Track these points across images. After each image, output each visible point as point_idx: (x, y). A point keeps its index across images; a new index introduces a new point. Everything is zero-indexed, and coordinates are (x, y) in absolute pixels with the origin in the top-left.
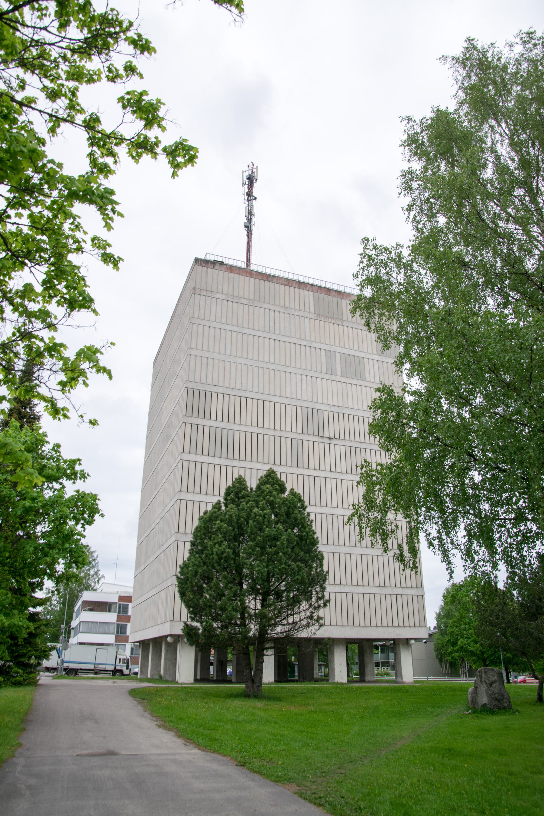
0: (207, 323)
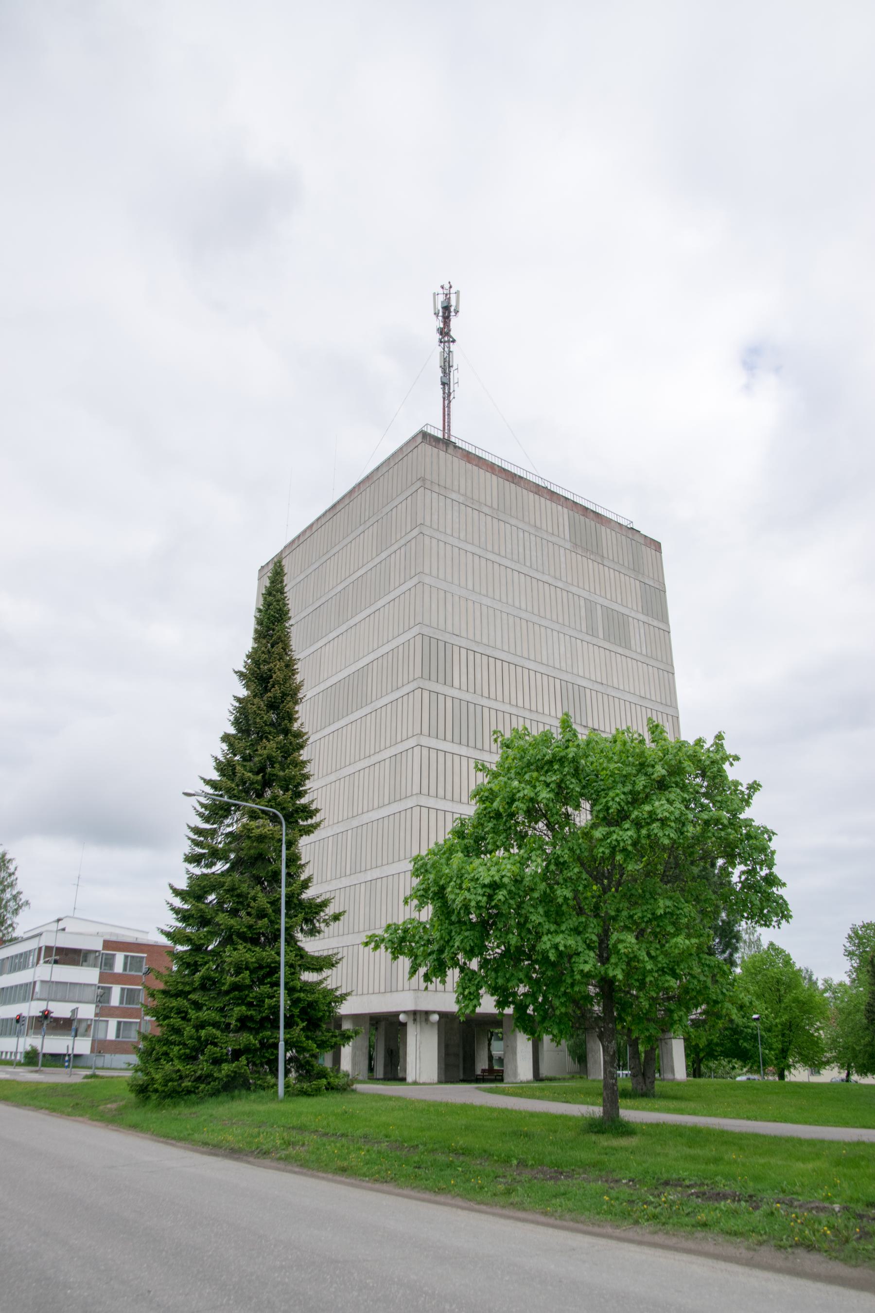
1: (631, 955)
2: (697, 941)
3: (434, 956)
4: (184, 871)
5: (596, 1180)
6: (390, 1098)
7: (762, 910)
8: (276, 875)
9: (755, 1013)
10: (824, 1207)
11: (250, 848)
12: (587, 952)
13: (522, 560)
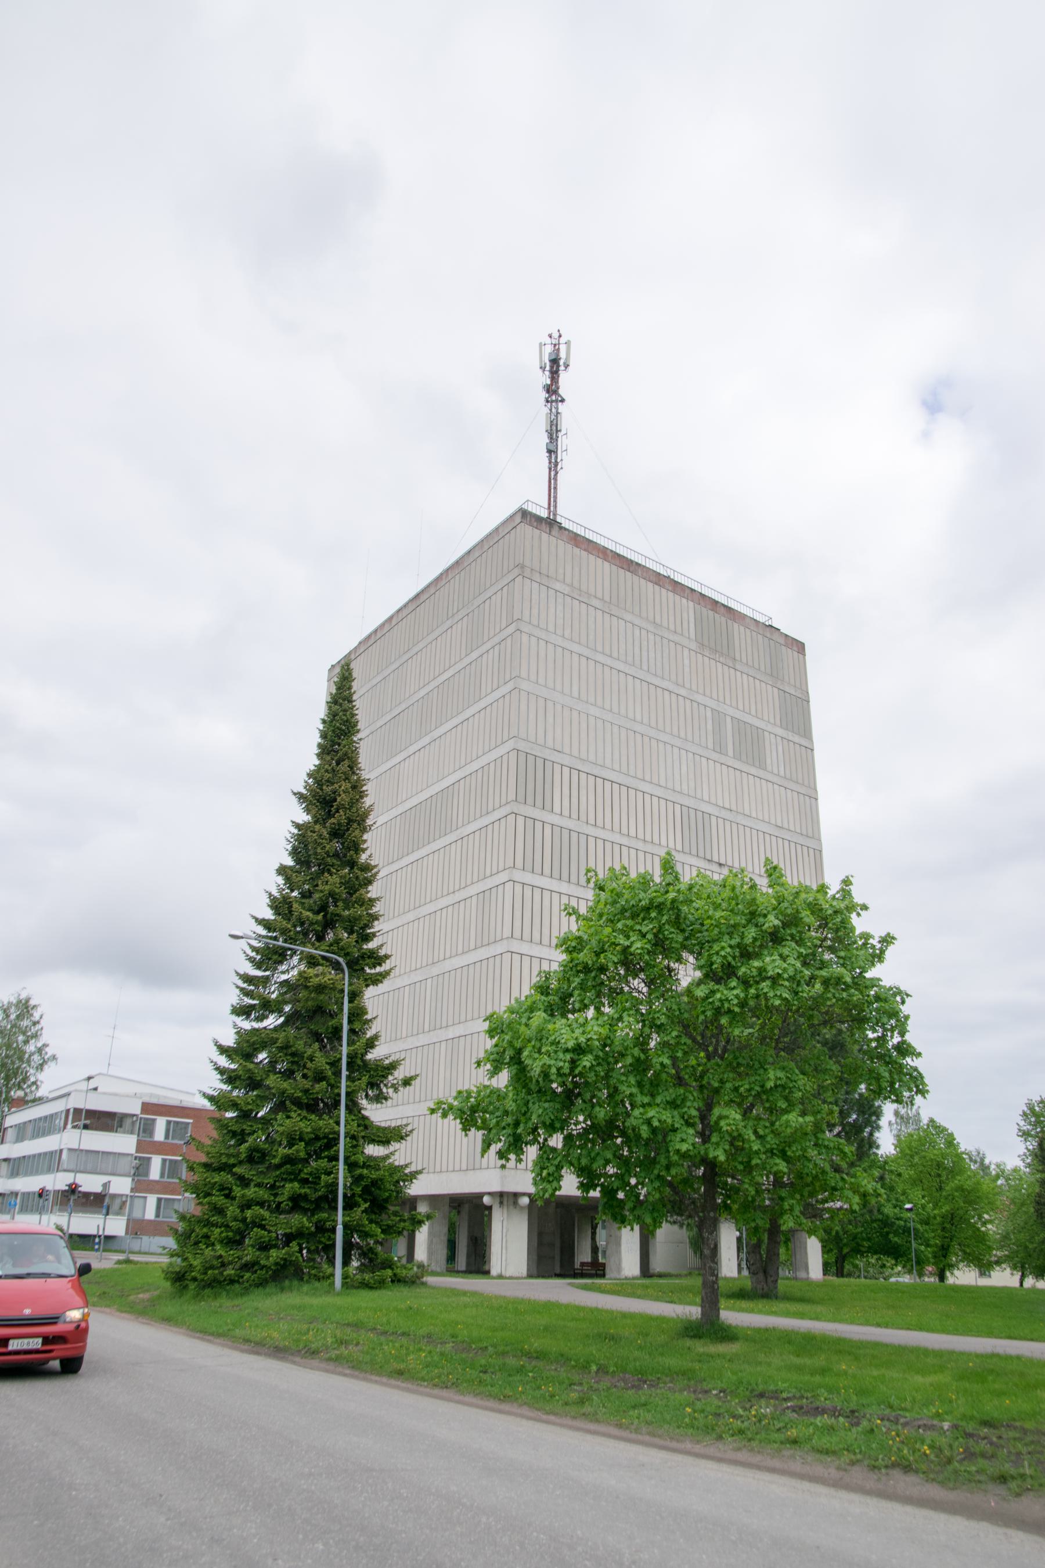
0: (543, 635)
1: (735, 1134)
2: (812, 1119)
3: (509, 1131)
4: (231, 1025)
5: (681, 1391)
6: (465, 1293)
7: (892, 1084)
8: (337, 1032)
9: (909, 1202)
10: (933, 1425)
11: (307, 1000)
12: (684, 1128)
13: (637, 662)
